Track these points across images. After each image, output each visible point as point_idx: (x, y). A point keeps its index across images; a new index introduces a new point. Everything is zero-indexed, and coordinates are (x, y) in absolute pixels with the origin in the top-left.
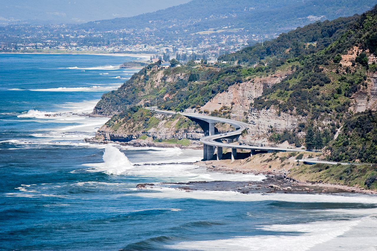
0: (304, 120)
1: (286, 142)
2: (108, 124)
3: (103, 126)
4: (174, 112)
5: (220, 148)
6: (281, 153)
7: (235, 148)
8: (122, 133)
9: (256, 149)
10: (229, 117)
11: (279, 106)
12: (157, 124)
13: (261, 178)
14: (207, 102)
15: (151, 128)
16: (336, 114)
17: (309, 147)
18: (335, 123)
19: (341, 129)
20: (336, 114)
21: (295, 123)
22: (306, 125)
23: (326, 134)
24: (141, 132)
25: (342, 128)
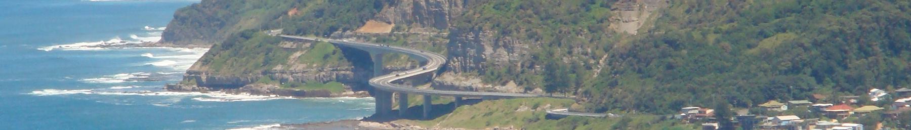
0: (538, 49)
1: (512, 82)
2: (205, 61)
3: (196, 63)
4: (312, 38)
5: (403, 96)
6: (784, 122)
7: (428, 95)
8: (224, 73)
9: (464, 96)
10: (405, 44)
11: (729, 4)
12: (287, 57)
13: (363, 118)
14: (367, 20)
15: (276, 64)
16: (590, 36)
17: (550, 89)
18: (589, 50)
19: (605, 60)
20: (590, 36)
21: (525, 52)
22: (542, 58)
23: (574, 68)
24: (259, 71)
25: (607, 58)
